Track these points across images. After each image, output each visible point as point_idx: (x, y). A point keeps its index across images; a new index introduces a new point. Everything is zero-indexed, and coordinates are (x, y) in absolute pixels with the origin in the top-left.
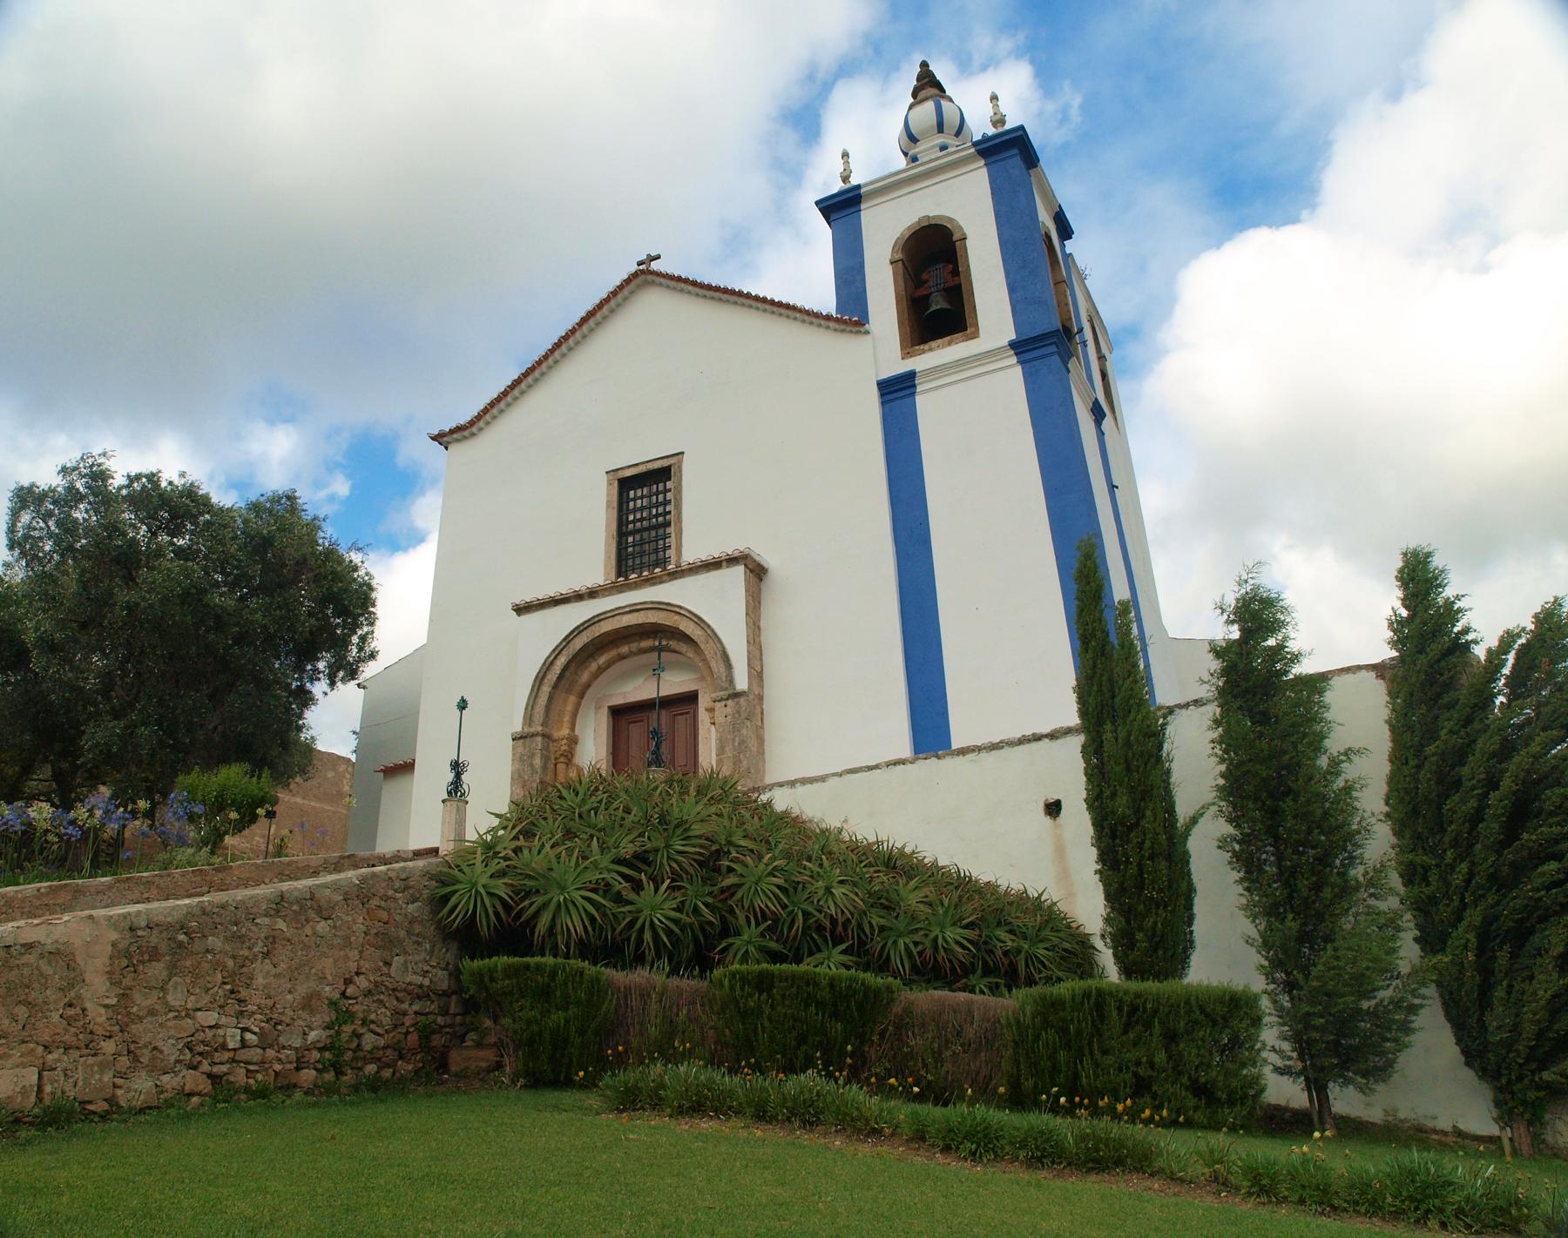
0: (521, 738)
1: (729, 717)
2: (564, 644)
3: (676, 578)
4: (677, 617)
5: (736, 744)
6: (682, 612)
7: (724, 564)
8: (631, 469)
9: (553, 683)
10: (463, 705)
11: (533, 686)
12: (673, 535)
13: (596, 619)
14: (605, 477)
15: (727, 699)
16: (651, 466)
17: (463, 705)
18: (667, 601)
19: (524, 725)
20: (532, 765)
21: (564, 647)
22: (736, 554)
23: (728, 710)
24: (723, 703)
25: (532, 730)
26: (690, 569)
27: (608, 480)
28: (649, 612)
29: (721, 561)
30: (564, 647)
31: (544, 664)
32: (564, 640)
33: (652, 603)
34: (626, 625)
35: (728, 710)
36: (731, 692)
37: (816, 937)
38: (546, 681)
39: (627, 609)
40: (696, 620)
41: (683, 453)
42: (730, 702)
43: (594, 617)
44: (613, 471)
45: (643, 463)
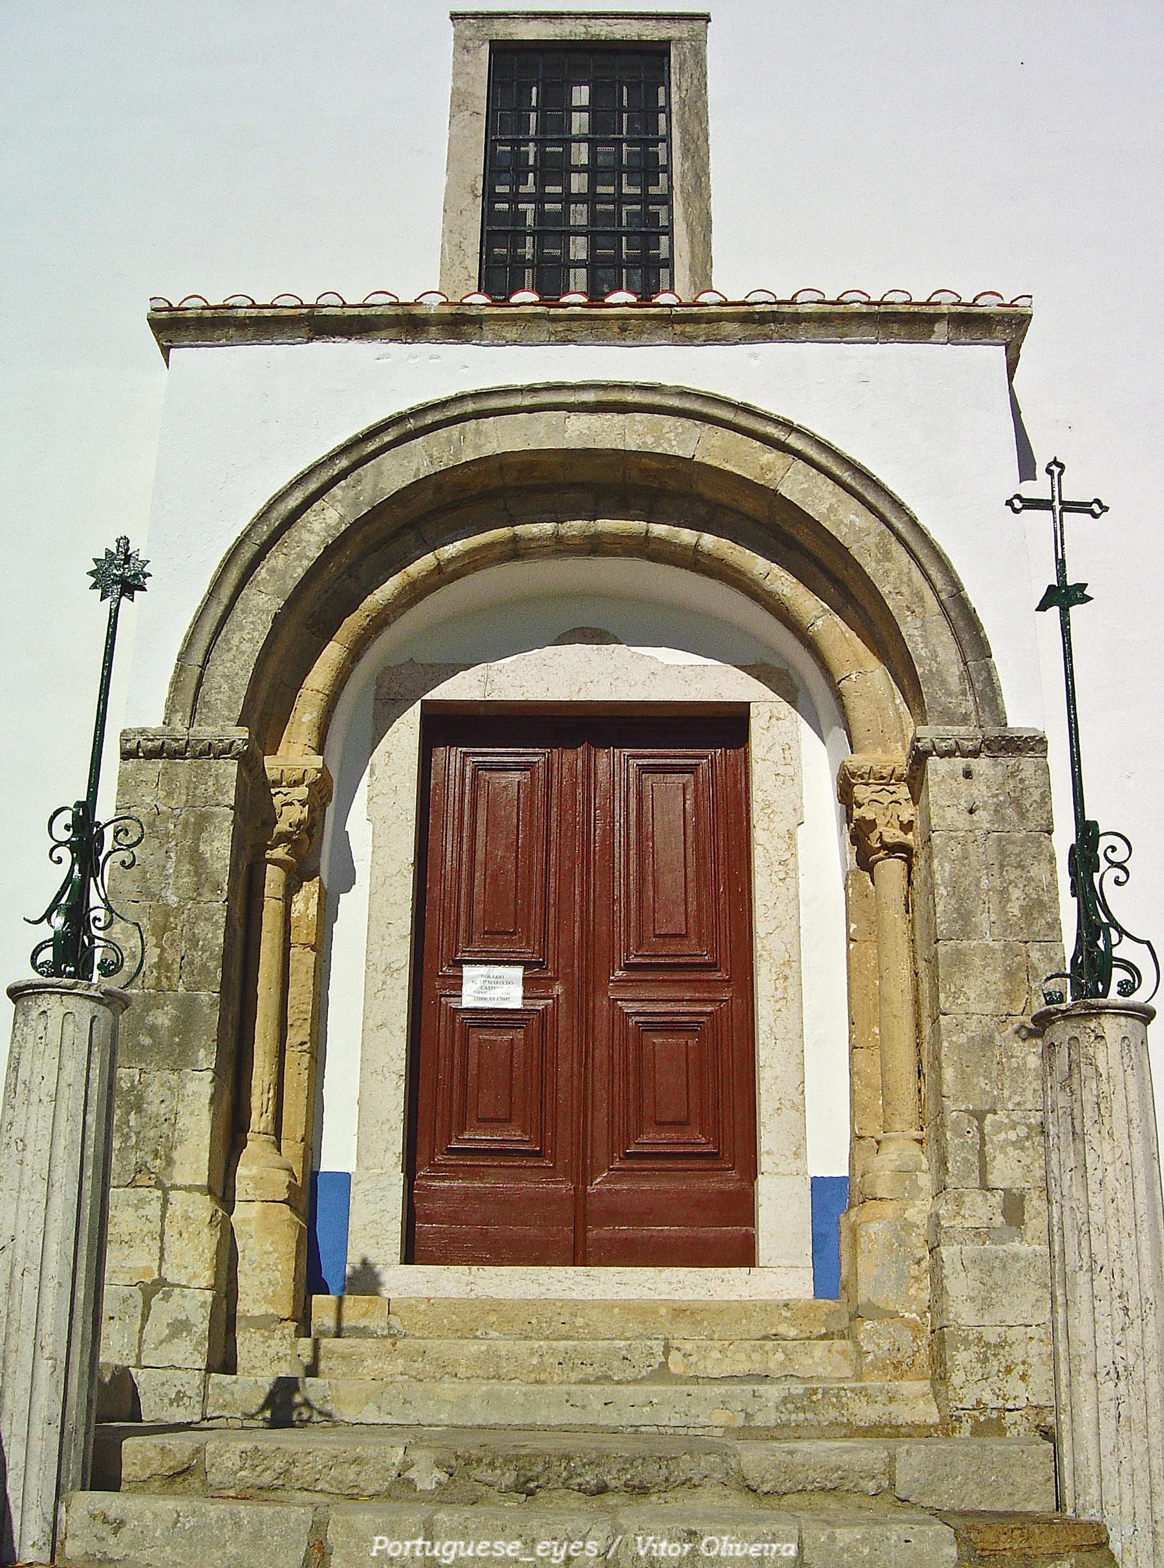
0: (153, 754)
1: (982, 815)
2: (343, 463)
3: (767, 338)
4: (770, 456)
5: (1014, 909)
6: (793, 441)
7: (941, 328)
8: (533, 24)
9: (291, 585)
10: (606, 1404)
11: (217, 584)
12: (680, 229)
13: (470, 407)
14: (449, 29)
15: (975, 754)
16: (601, 30)
17: (606, 1404)
18: (737, 398)
19: (171, 708)
20: (196, 859)
21: (343, 474)
22: (989, 305)
23: (979, 790)
24: (959, 763)
25: (206, 732)
26: (823, 319)
27: (457, 38)
28: (669, 421)
29: (934, 318)
30: (343, 474)
31: (263, 516)
32: (344, 450)
33: (683, 393)
34: (579, 445)
35: (979, 790)
36: (993, 731)
37: (631, 1080)
38: (262, 573)
39: (590, 397)
40: (847, 477)
41: (706, 18)
42: (981, 764)
43: (461, 398)
44: (475, 16)
45: (577, 16)
